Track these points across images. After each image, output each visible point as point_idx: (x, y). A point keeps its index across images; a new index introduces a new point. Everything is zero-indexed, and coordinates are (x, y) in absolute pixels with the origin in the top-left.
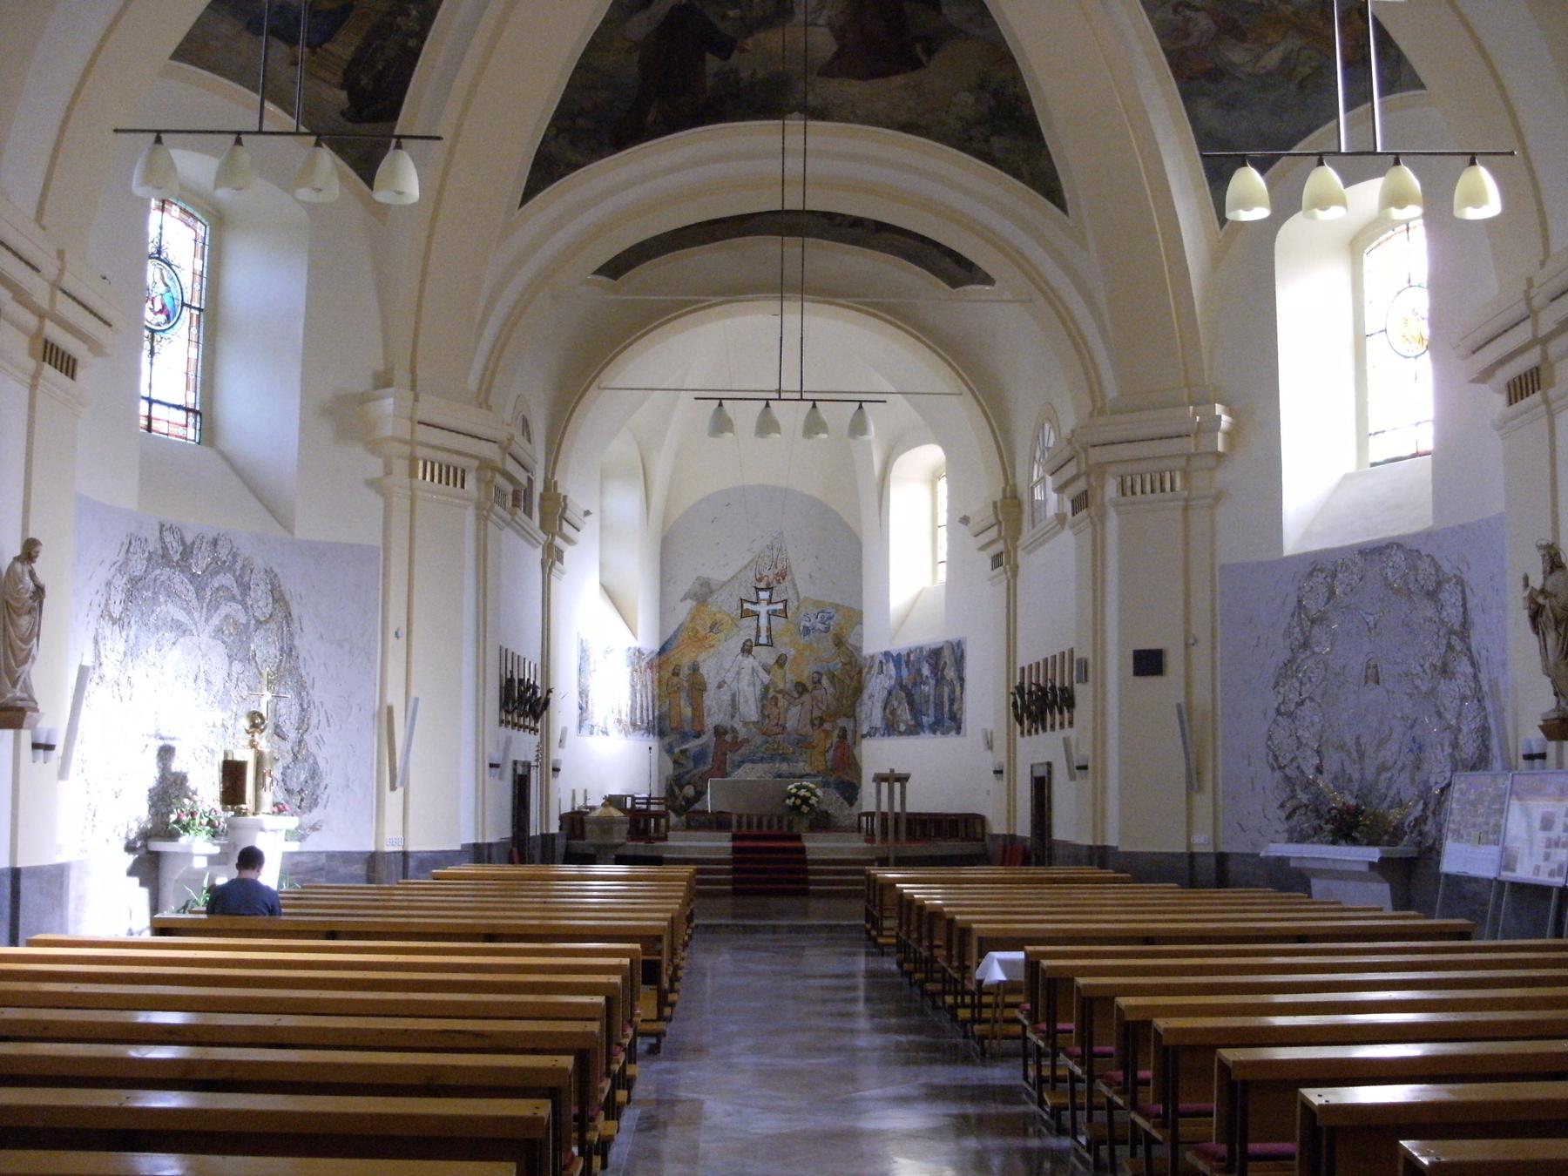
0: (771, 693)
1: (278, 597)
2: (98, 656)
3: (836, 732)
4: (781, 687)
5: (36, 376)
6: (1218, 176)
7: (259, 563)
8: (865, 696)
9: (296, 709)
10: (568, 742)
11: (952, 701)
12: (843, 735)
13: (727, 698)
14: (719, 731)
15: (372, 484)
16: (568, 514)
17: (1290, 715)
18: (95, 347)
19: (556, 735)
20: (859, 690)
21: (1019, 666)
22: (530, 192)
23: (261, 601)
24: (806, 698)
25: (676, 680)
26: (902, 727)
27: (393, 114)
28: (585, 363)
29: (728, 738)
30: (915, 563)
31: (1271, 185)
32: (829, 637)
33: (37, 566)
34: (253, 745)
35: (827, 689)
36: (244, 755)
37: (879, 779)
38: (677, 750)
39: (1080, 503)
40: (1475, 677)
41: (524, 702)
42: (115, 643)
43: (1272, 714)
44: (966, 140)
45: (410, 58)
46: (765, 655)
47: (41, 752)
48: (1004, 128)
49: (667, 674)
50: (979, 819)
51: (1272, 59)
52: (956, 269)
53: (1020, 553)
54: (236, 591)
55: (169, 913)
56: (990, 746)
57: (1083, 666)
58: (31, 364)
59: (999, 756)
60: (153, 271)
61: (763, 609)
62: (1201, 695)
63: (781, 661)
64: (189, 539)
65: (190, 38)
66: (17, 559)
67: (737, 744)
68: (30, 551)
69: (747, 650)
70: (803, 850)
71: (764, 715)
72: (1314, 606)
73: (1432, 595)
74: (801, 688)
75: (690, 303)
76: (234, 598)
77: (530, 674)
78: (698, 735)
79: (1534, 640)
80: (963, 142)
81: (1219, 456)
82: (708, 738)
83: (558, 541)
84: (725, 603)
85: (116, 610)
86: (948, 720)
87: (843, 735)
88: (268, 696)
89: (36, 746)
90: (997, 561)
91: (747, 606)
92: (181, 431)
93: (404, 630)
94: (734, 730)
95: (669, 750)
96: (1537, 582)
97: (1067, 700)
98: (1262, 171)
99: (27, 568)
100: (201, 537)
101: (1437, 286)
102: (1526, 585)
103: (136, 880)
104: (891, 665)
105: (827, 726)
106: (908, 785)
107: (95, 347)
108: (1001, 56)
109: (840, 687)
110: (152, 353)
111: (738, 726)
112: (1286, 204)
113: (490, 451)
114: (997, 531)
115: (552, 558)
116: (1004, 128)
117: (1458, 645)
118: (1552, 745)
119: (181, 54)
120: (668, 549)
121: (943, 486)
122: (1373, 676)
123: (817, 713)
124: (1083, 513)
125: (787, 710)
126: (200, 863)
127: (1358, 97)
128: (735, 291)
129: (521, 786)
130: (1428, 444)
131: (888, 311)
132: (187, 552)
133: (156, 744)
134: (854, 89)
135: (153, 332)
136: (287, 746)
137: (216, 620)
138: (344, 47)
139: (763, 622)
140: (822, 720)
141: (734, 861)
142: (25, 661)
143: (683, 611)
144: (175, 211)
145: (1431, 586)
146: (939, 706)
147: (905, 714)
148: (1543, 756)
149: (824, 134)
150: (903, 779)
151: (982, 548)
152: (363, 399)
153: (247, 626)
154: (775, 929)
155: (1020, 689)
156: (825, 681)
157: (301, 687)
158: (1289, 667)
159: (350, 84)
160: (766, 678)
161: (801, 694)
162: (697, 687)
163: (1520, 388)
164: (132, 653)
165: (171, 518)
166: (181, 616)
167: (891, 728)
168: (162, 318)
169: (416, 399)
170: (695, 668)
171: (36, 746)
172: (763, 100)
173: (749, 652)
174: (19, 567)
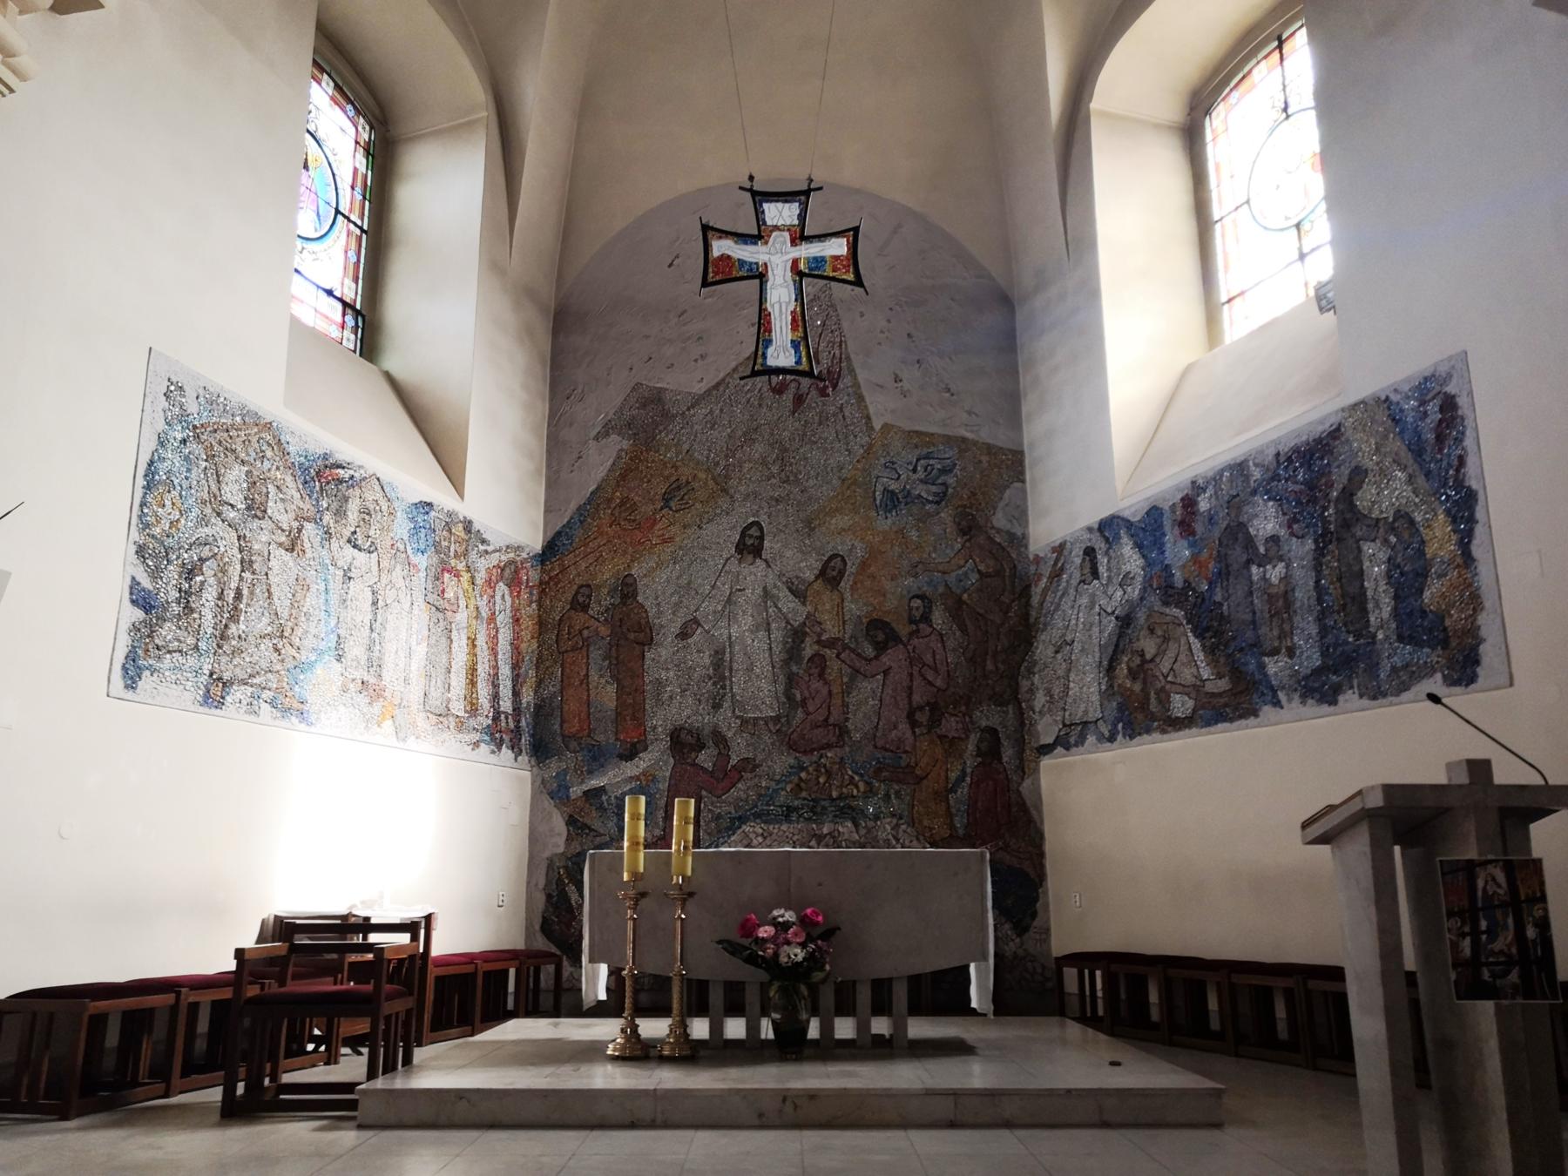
0: (809, 650)
3: (974, 738)
4: (831, 630)
8: (1043, 649)
20: (1024, 634)
24: (894, 658)
25: (579, 619)
26: (1181, 705)
29: (706, 759)
32: (946, 515)
35: (945, 640)
38: (576, 791)
46: (792, 556)
49: (560, 606)
61: (777, 257)
63: (831, 573)
69: (750, 546)
74: (880, 633)
78: (630, 754)
91: (720, 247)
94: (720, 739)
95: (552, 791)
104: (1127, 549)
105: (950, 725)
111: (725, 720)
125: (847, 690)
139: (781, 296)
143: (599, 463)
147: (1189, 661)
156: (939, 618)
161: (881, 648)
162: (631, 633)
167: (1138, 711)
170: (627, 590)
173: (757, 551)
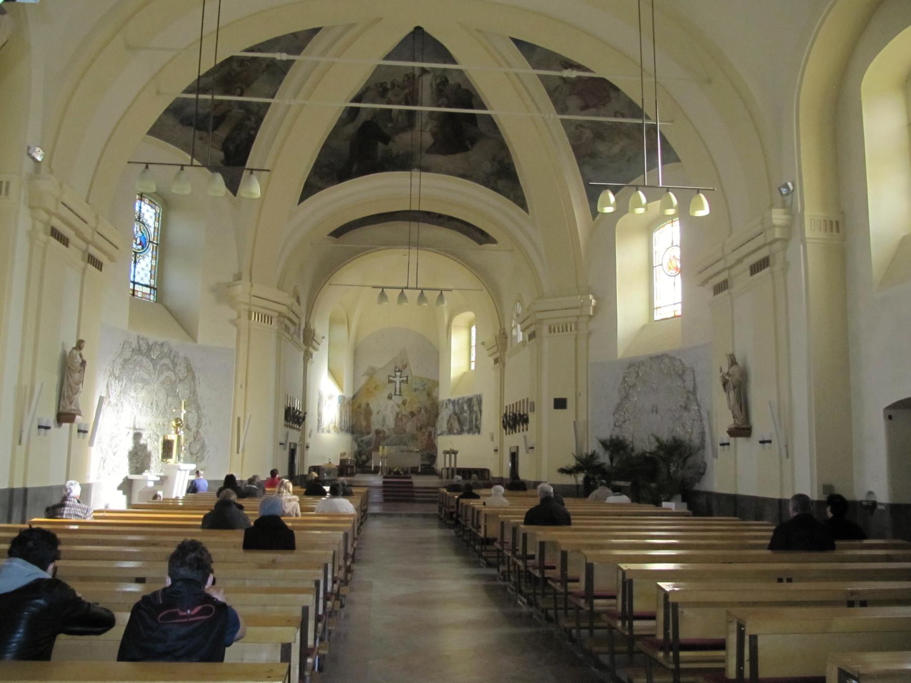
1: (189, 369)
2: (108, 392)
5: (84, 271)
6: (593, 195)
7: (181, 354)
9: (196, 418)
10: (313, 435)
11: (476, 420)
12: (430, 435)
13: (381, 418)
14: (378, 432)
15: (233, 322)
16: (316, 338)
17: (620, 427)
18: (111, 258)
19: (308, 432)
20: (437, 415)
21: (506, 404)
22: (302, 199)
23: (182, 369)
24: (415, 418)
27: (244, 163)
28: (325, 271)
29: (381, 435)
30: (462, 356)
31: (616, 199)
33: (83, 352)
34: (177, 432)
36: (172, 437)
37: (446, 452)
39: (532, 336)
40: (699, 410)
41: (295, 418)
42: (116, 387)
43: (612, 426)
44: (488, 182)
45: (251, 140)
46: (398, 400)
47: (81, 434)
48: (503, 177)
50: (487, 471)
51: (616, 149)
52: (481, 236)
53: (506, 358)
54: (171, 366)
55: (135, 501)
56: (492, 439)
57: (533, 404)
58: (82, 264)
59: (496, 444)
60: (136, 227)
61: (398, 380)
62: (582, 417)
63: (404, 403)
64: (150, 343)
65: (155, 126)
66: (74, 348)
67: (384, 438)
68: (80, 345)
69: (390, 397)
70: (411, 483)
71: (396, 425)
72: (631, 380)
73: (681, 376)
74: (412, 414)
75: (368, 249)
76: (170, 369)
77: (297, 405)
78: (368, 434)
79: (724, 395)
80: (486, 183)
81: (590, 317)
82: (372, 435)
83: (311, 349)
84: (381, 378)
85: (117, 373)
86: (475, 428)
87: (430, 435)
88: (184, 412)
89: (79, 431)
90: (496, 361)
92: (148, 297)
93: (244, 386)
95: (356, 440)
96: (725, 370)
97: (524, 420)
98: (614, 194)
99: (78, 353)
100: (156, 343)
101: (682, 246)
102: (721, 371)
103: (121, 492)
105: (424, 430)
106: (458, 455)
107: (111, 258)
108: (502, 146)
109: (428, 414)
110: (135, 262)
111: (385, 429)
112: (622, 209)
113: (284, 309)
114: (498, 348)
115: (308, 356)
116: (503, 177)
117: (692, 398)
118: (732, 439)
119: (151, 132)
120: (356, 353)
121: (474, 329)
122: (655, 410)
123: (419, 425)
124: (533, 340)
126: (151, 484)
127: (653, 165)
128: (391, 244)
129: (292, 453)
130: (679, 313)
131: (452, 254)
132: (150, 349)
133: (132, 432)
134: (440, 159)
135: (136, 253)
136: (192, 434)
137: (162, 378)
138: (223, 133)
140: (421, 428)
141: (384, 487)
142: (76, 393)
143: (363, 380)
144: (147, 201)
145: (680, 372)
146: (471, 422)
147: (456, 426)
148: (728, 444)
149: (428, 179)
150: (455, 453)
151: (491, 355)
152: (229, 286)
153: (175, 382)
154: (401, 515)
155: (505, 415)
156: (423, 411)
157: (198, 408)
158: (619, 408)
159: (225, 149)
160: (398, 410)
162: (368, 413)
163: (721, 287)
164: (123, 392)
165: (145, 335)
166: (146, 377)
167: (450, 431)
168: (140, 247)
169: (252, 286)
170: (368, 405)
171: (79, 431)
172: (401, 163)
174: (75, 352)
